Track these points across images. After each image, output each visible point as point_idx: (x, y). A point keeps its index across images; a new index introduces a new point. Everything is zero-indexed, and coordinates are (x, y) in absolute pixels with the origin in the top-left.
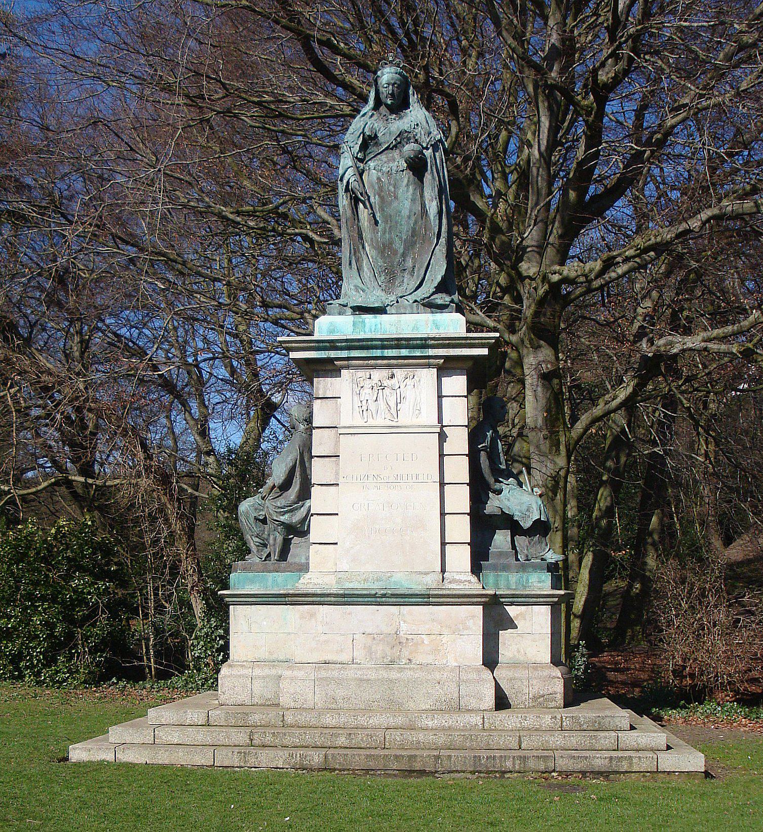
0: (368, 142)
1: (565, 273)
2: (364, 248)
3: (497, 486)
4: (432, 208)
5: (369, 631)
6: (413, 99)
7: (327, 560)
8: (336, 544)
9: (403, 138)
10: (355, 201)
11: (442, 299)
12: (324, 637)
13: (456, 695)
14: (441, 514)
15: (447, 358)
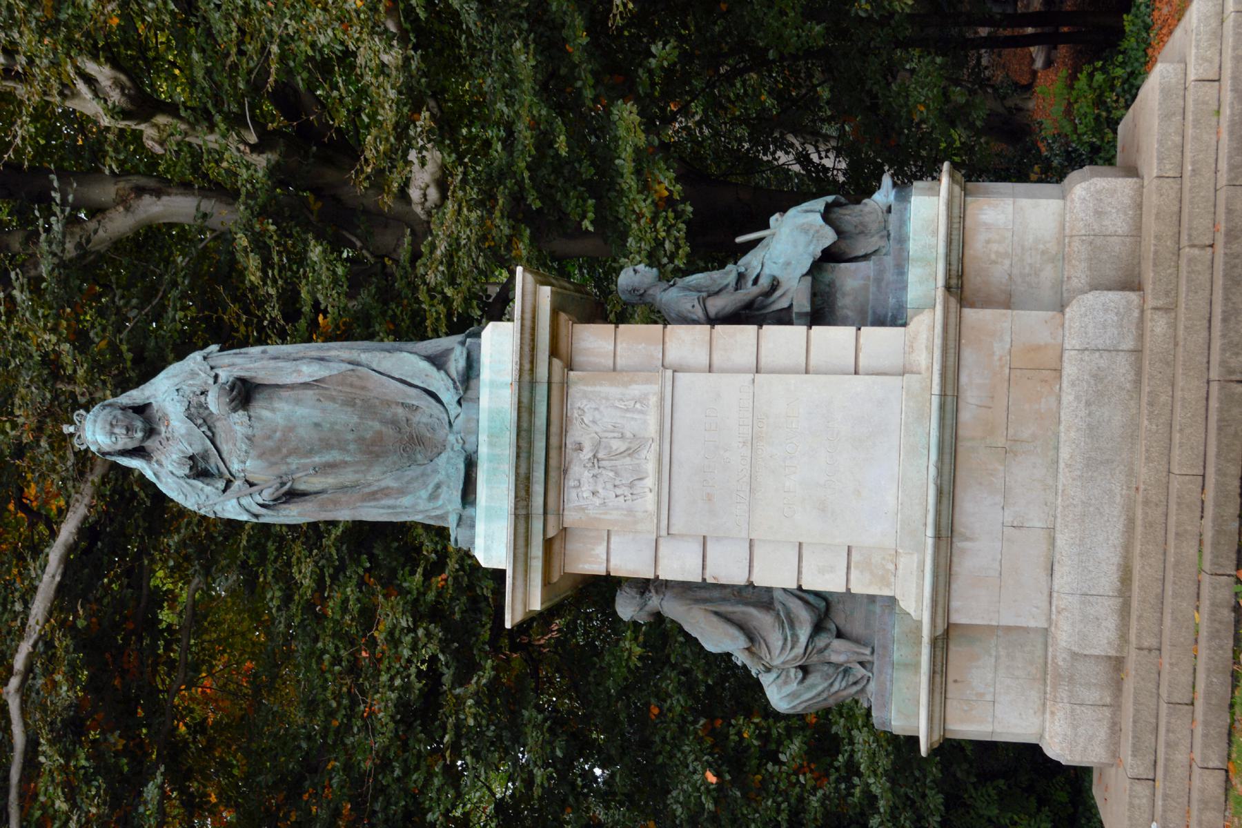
0: (199, 470)
3: (764, 282)
10: (292, 495)
15: (554, 352)
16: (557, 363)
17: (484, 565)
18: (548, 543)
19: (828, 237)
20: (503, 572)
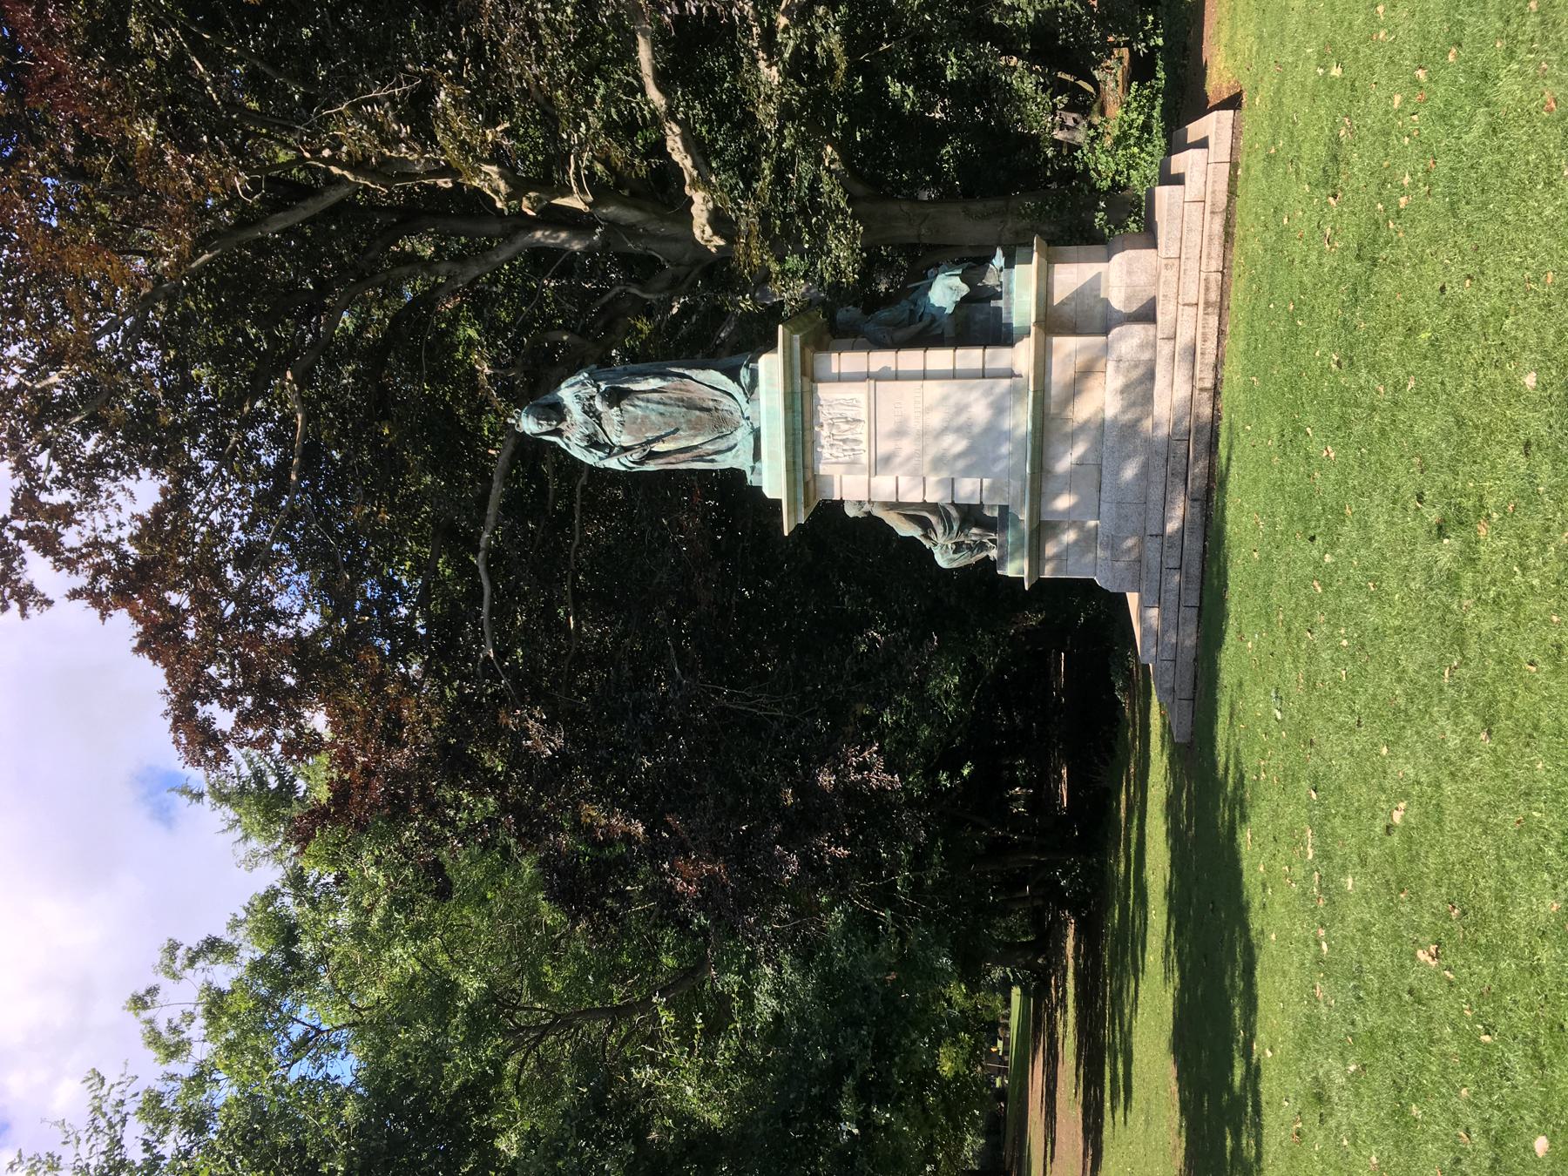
0: (593, 443)
1: (704, 221)
2: (696, 447)
3: (927, 320)
4: (655, 383)
9: (590, 411)
10: (653, 455)
11: (744, 375)
14: (954, 377)
15: (803, 374)
16: (806, 380)
17: (769, 496)
18: (806, 484)
19: (965, 290)
20: (779, 502)
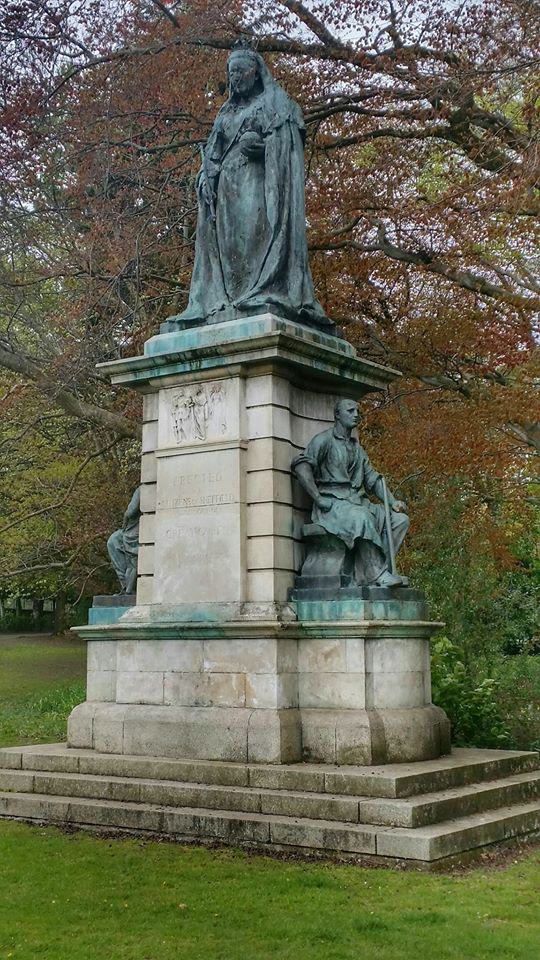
3: (324, 502)
5: (176, 668)
6: (267, 80)
7: (162, 590)
8: (152, 575)
12: (140, 676)
13: (244, 744)
15: (246, 365)
